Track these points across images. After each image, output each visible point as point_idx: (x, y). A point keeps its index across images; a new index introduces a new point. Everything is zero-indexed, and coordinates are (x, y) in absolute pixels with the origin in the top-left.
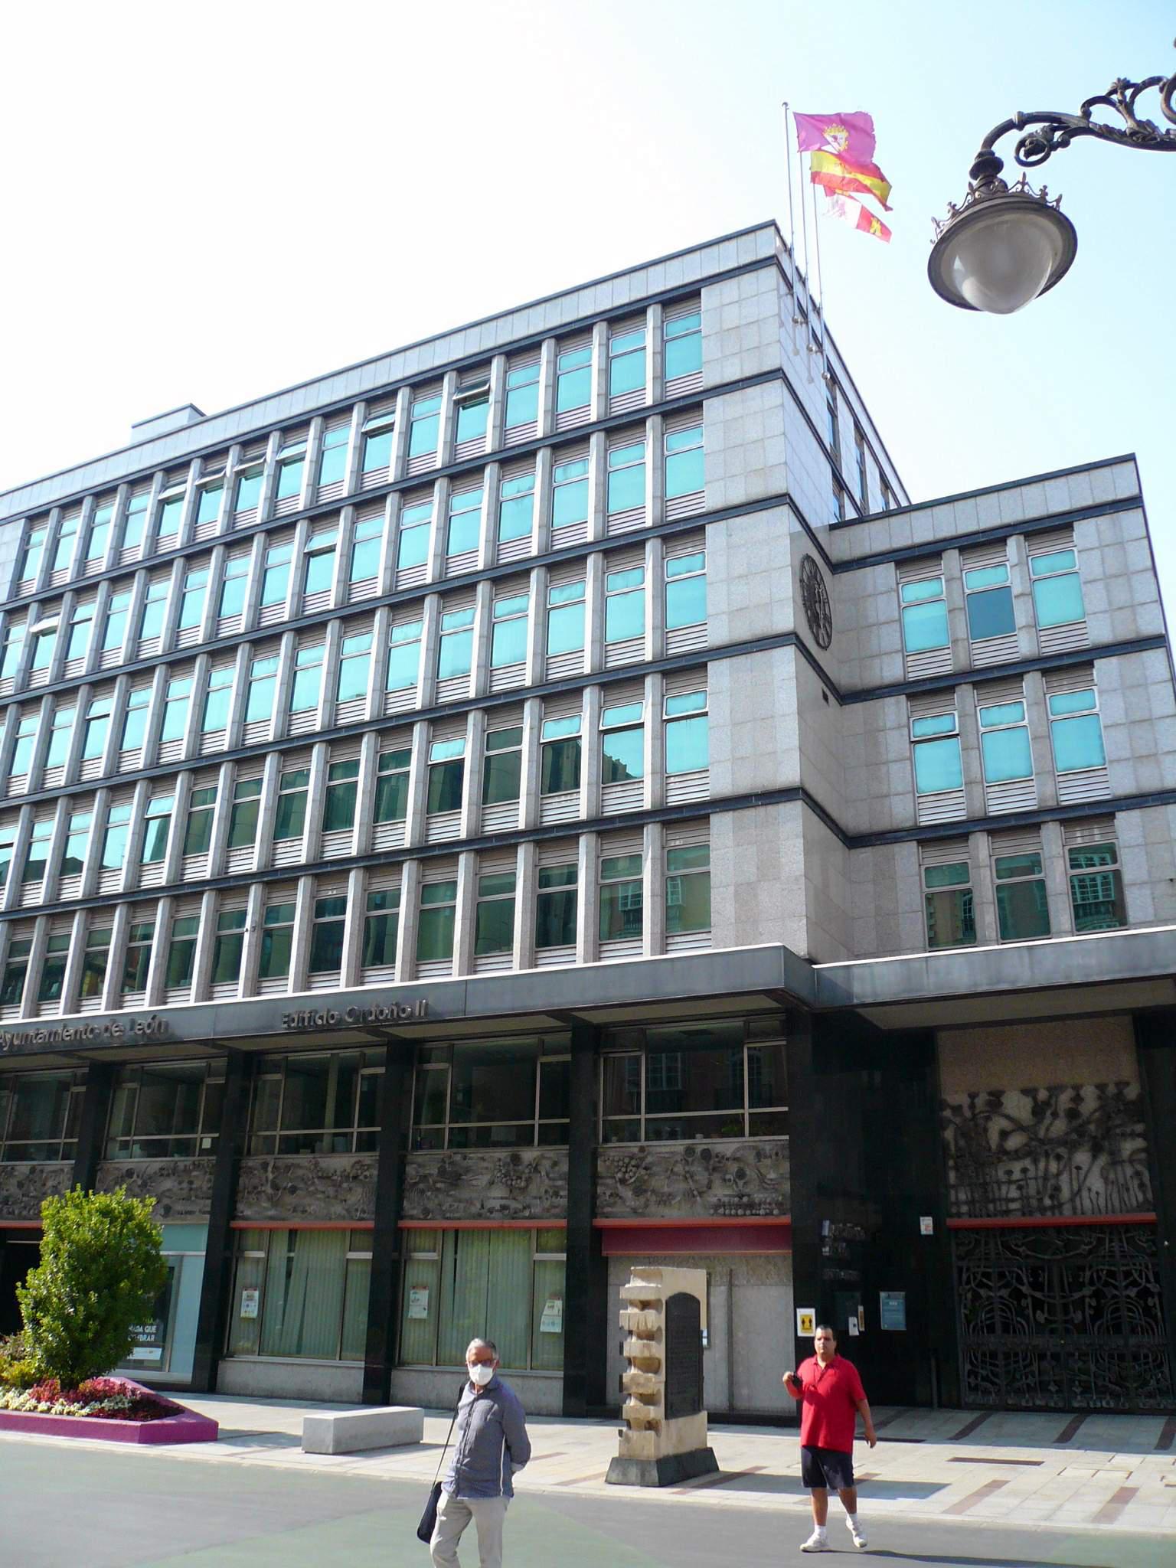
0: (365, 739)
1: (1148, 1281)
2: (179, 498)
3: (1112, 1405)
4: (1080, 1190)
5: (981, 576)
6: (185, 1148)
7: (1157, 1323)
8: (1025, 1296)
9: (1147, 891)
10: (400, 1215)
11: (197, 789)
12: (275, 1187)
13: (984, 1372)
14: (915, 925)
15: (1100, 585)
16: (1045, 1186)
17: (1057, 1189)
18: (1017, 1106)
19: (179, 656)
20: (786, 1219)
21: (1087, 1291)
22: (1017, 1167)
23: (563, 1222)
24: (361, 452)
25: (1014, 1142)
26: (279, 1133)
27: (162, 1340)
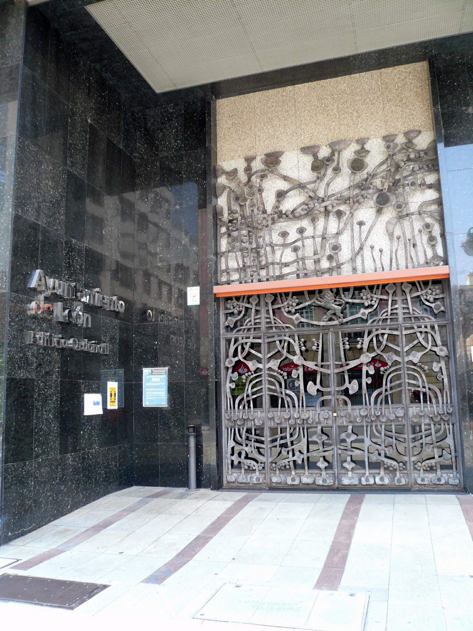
3: (387, 481)
4: (361, 248)
7: (442, 390)
8: (296, 366)
16: (323, 247)
17: (336, 248)
21: (365, 358)
22: (292, 228)
25: (292, 202)
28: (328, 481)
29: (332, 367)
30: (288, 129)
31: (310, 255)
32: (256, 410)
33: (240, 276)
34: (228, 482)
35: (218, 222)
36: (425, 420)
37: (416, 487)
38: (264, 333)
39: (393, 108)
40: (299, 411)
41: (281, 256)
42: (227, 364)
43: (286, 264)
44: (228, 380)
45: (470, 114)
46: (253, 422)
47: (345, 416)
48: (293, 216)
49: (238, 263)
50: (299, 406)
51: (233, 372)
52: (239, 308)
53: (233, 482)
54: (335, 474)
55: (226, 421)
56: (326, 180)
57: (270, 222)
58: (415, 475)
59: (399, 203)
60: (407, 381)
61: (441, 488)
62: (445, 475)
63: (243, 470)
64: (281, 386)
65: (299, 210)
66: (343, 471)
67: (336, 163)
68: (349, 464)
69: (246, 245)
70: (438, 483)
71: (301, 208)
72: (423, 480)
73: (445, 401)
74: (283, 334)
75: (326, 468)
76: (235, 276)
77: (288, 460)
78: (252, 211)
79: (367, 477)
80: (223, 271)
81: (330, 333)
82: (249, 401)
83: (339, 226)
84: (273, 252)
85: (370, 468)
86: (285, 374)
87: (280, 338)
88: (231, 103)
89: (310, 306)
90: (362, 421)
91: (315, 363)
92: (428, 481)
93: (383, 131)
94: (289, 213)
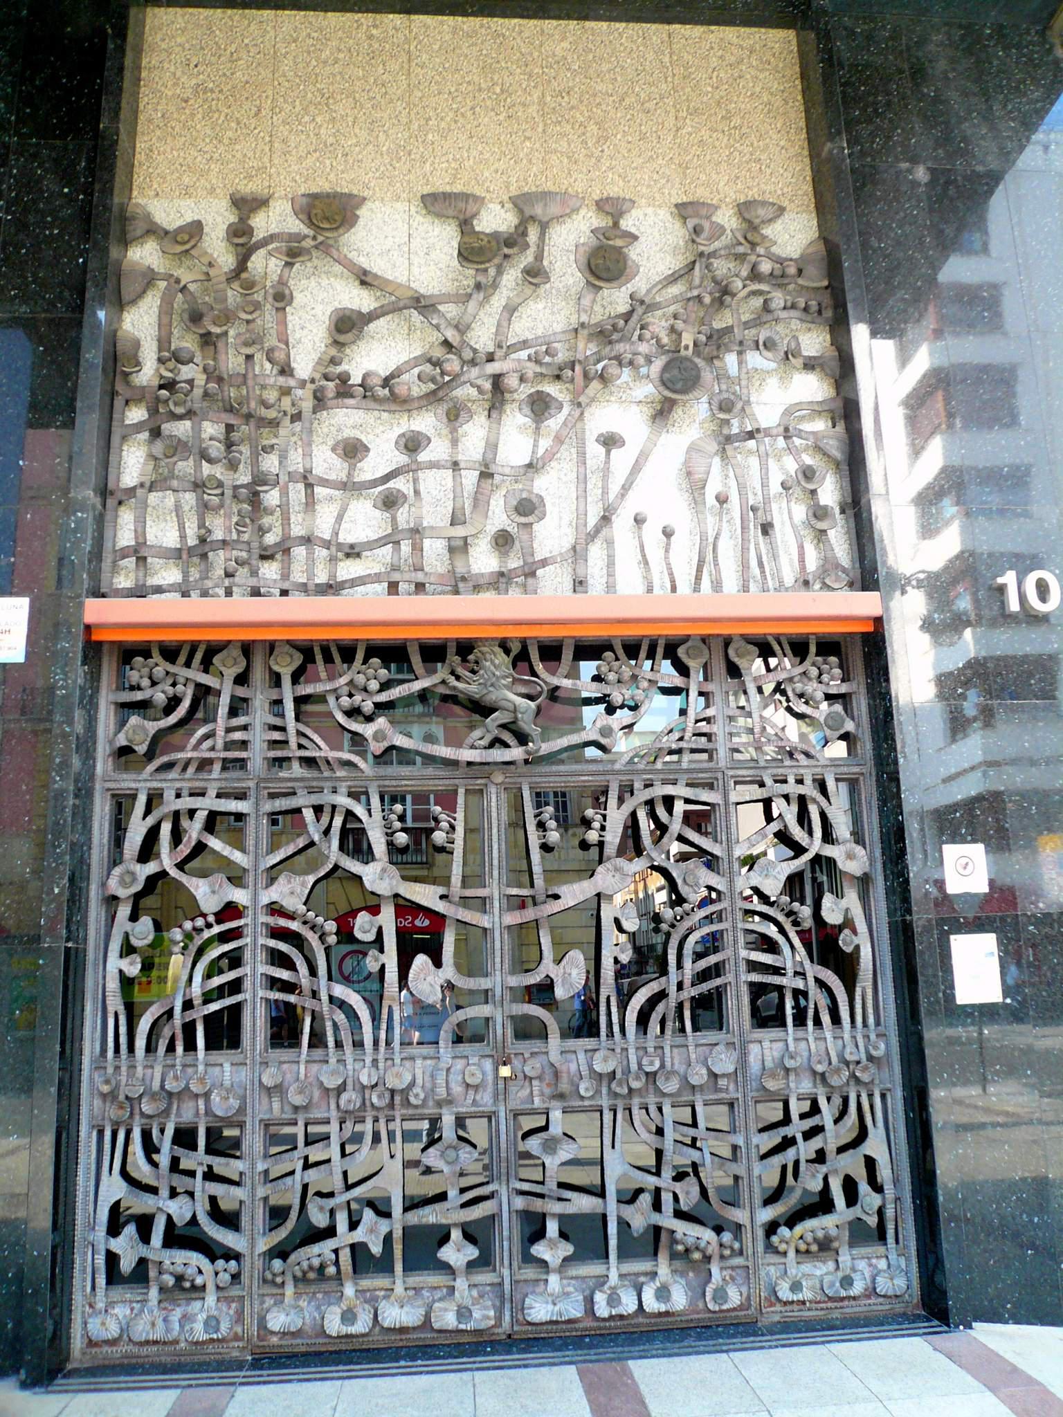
1: (828, 837)
2: (698, 956)
3: (679, 1300)
4: (606, 519)
13: (179, 1210)
16: (480, 501)
17: (527, 508)
18: (402, 243)
22: (382, 438)
28: (477, 1314)
29: (496, 904)
30: (382, 137)
31: (442, 525)
32: (216, 1056)
33: (186, 574)
34: (91, 1343)
35: (119, 387)
36: (798, 1082)
37: (774, 1315)
38: (261, 780)
39: (705, 133)
40: (375, 1061)
41: (340, 518)
42: (114, 886)
43: (352, 546)
44: (115, 946)
45: (919, 185)
46: (201, 1103)
47: (540, 1078)
48: (385, 393)
49: (182, 528)
50: (376, 1043)
51: (134, 917)
52: (174, 685)
53: (113, 1342)
54: (501, 1284)
55: (97, 1102)
56: (498, 301)
57: (307, 405)
58: (770, 1269)
59: (725, 395)
60: (744, 953)
61: (851, 1309)
62: (862, 1265)
63: (154, 1293)
64: (313, 972)
65: (410, 377)
66: (530, 1273)
67: (530, 259)
68: (552, 1245)
69: (218, 471)
70: (843, 1293)
71: (416, 371)
72: (796, 1287)
73: (859, 1019)
74: (327, 785)
75: (471, 1265)
76: (169, 575)
77: (331, 1244)
78: (249, 358)
79: (613, 1288)
80: (124, 553)
81: (493, 789)
82: (193, 1022)
83: (535, 446)
84: (310, 503)
85: (623, 1255)
86: (331, 926)
87: (315, 799)
88: (198, 26)
89: (423, 696)
90: (598, 1092)
91: (441, 890)
92: (812, 1288)
93: (674, 192)
94: (376, 381)
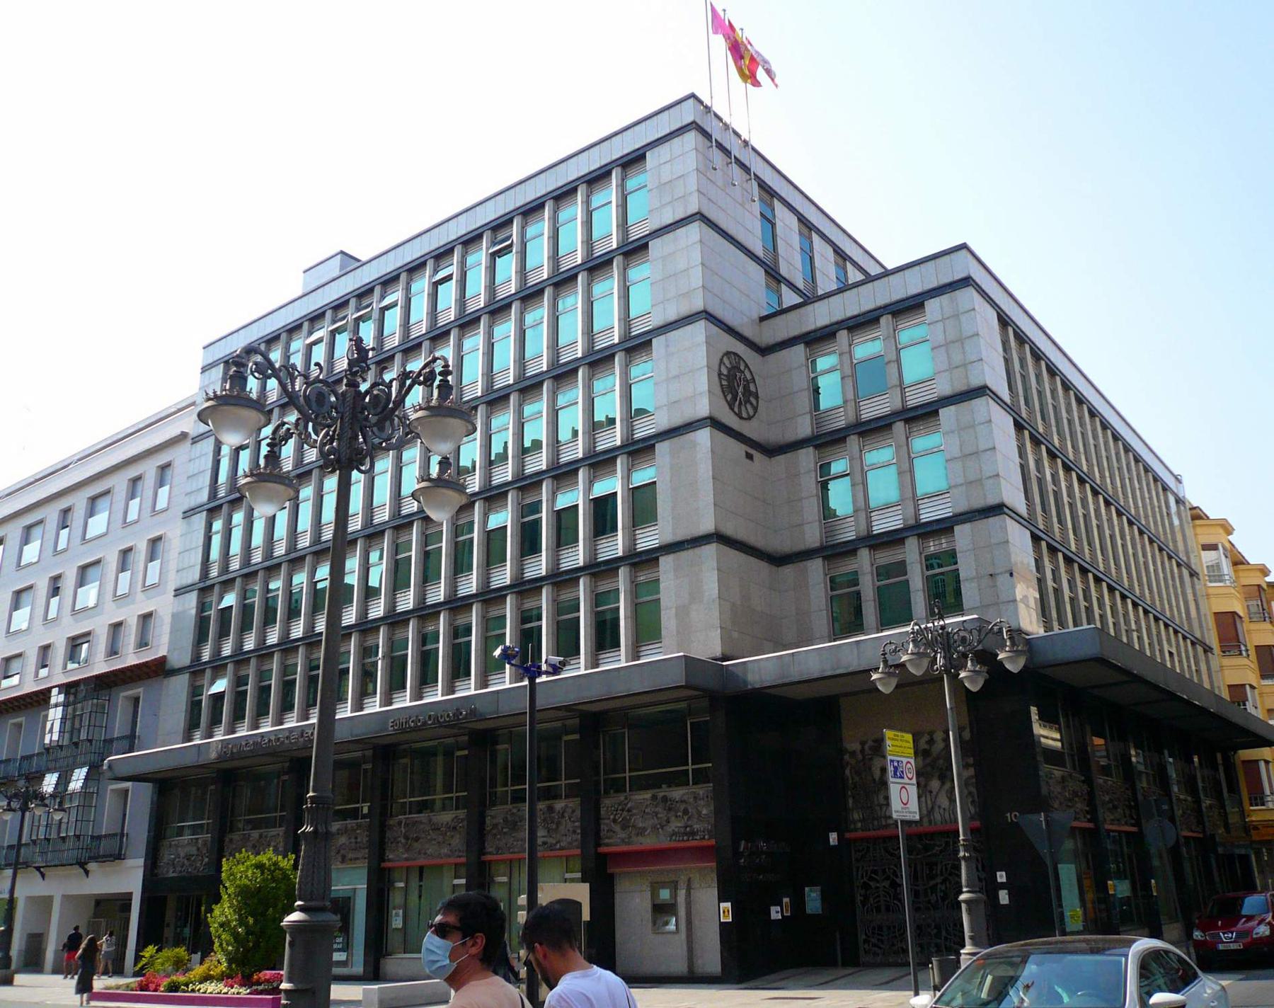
0: (619, 461)
2: (394, 305)
5: (867, 347)
6: (354, 814)
9: (974, 585)
10: (482, 851)
11: (460, 523)
12: (407, 838)
14: (821, 621)
15: (943, 350)
19: (528, 383)
20: (713, 842)
21: (939, 880)
23: (578, 851)
24: (492, 269)
26: (510, 788)
27: (347, 947)
76: (859, 825)
